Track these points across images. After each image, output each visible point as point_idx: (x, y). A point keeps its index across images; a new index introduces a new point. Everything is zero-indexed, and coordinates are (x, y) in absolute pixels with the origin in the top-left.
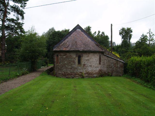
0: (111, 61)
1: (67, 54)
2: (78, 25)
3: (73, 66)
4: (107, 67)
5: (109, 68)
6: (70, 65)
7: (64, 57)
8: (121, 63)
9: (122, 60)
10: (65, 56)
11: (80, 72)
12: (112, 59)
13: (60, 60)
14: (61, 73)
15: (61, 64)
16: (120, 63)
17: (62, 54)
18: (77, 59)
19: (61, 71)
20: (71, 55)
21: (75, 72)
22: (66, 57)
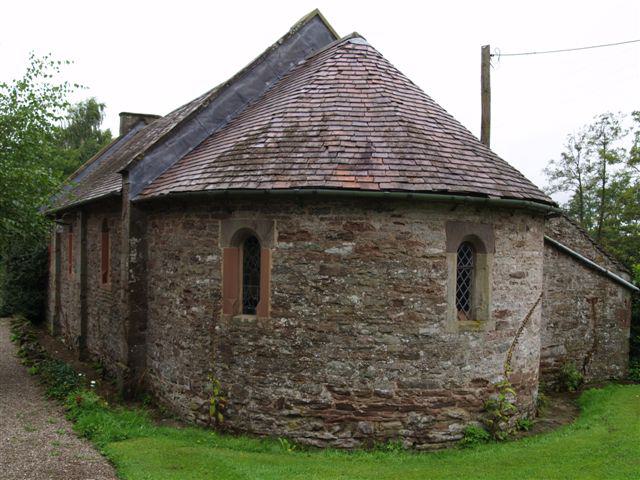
0: (575, 286)
1: (371, 228)
2: (317, 16)
3: (422, 331)
4: (556, 324)
5: (563, 326)
6: (398, 322)
7: (334, 250)
8: (621, 295)
9: (624, 275)
10: (346, 237)
11: (477, 381)
12: (78, 291)
13: (279, 278)
14: (298, 396)
15: (295, 316)
16: (614, 294)
17: (314, 224)
18: (452, 263)
19: (300, 379)
20: (404, 229)
21: (439, 379)
22: (358, 250)
